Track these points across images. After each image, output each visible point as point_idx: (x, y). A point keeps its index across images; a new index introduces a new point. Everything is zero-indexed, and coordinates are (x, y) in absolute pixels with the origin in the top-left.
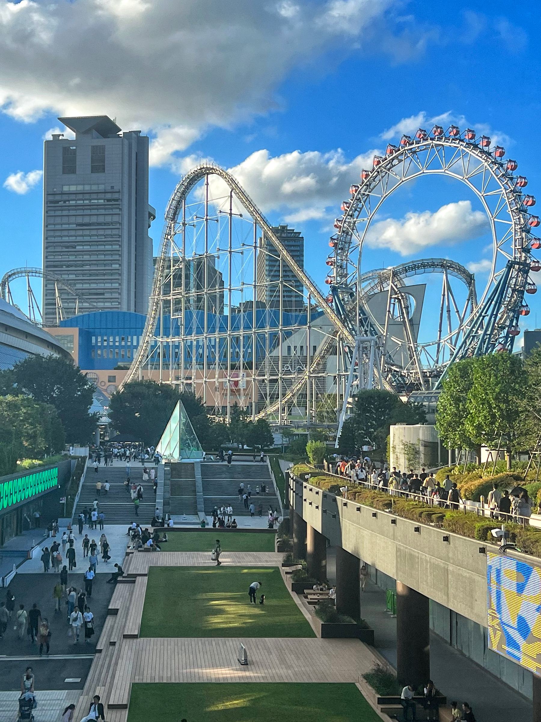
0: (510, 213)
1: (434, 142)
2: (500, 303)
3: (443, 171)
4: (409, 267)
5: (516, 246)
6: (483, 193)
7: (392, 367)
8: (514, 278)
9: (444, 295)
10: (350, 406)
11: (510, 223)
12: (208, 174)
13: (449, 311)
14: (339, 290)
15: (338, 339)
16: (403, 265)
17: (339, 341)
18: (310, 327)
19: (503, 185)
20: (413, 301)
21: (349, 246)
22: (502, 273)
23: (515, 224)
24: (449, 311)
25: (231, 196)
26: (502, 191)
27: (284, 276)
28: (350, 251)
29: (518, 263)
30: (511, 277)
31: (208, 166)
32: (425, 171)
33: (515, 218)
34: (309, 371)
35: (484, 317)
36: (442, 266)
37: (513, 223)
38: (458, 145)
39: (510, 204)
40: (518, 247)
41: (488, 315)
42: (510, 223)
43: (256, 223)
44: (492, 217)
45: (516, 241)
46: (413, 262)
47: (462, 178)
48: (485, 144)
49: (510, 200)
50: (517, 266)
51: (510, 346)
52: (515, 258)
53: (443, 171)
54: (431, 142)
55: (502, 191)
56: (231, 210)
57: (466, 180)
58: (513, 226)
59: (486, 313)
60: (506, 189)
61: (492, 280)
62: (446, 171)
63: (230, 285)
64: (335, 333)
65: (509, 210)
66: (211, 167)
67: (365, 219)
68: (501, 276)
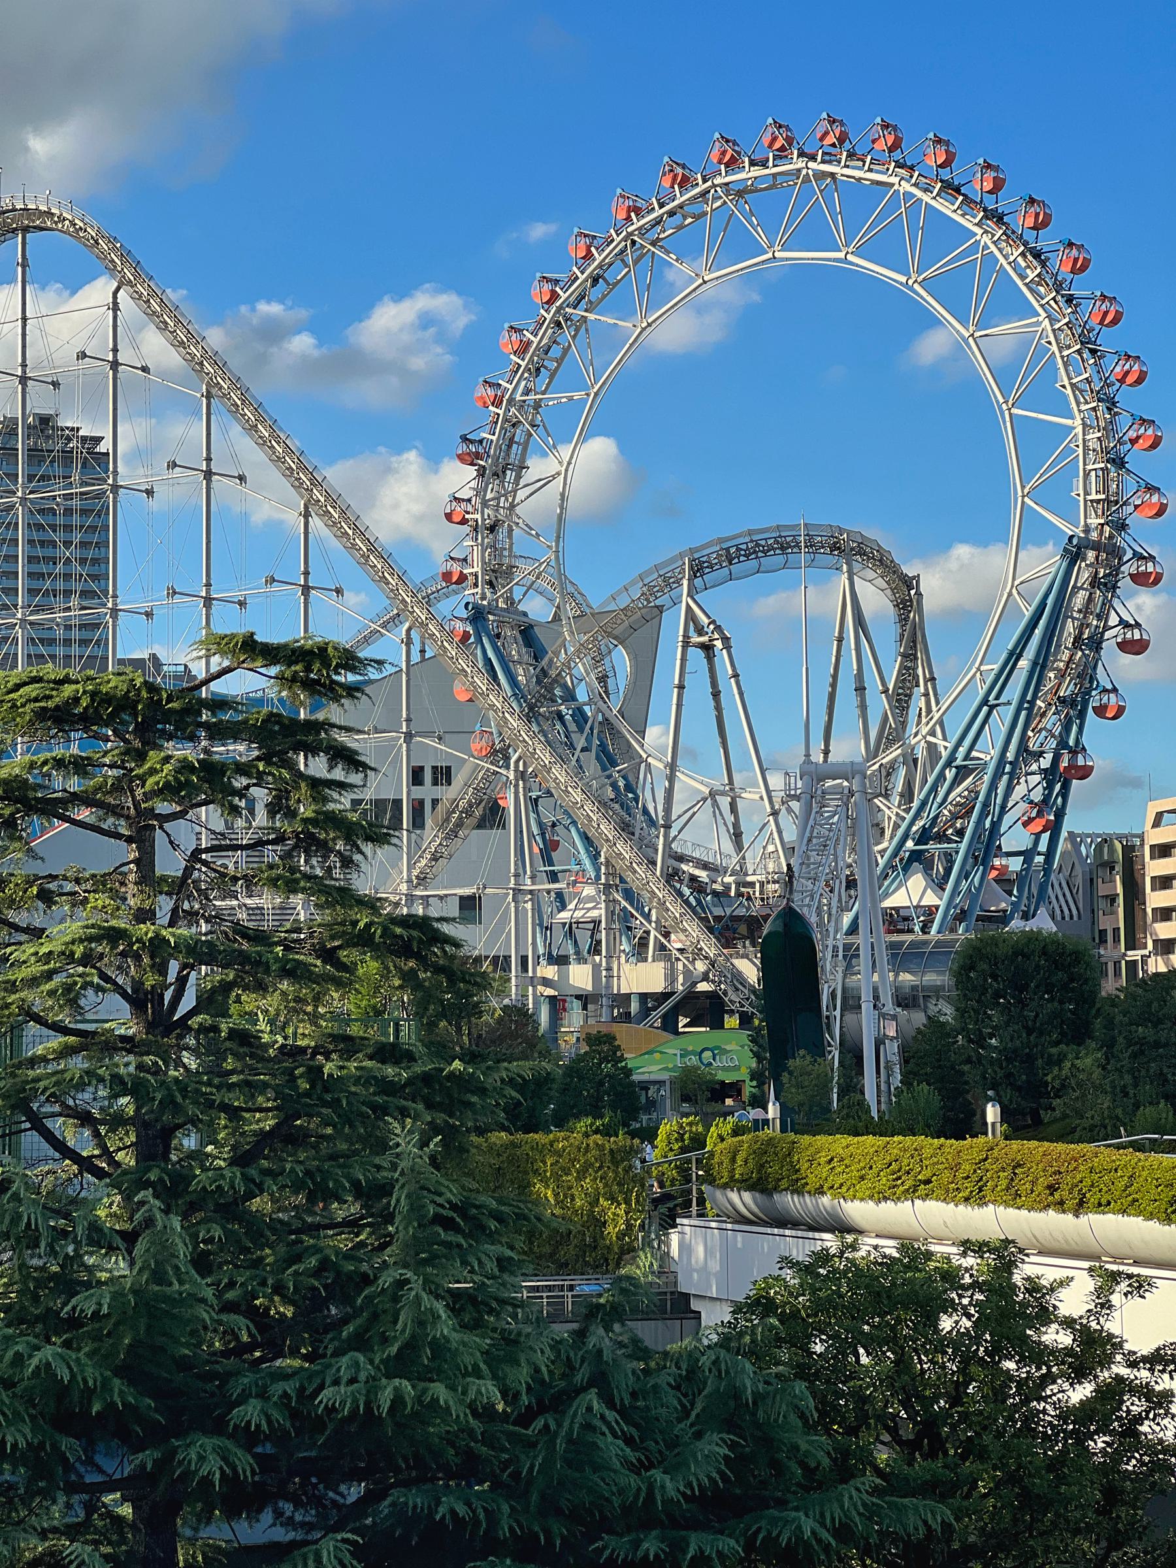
0: (1069, 391)
1: (811, 165)
2: (1043, 667)
3: (841, 255)
4: (738, 550)
5: (1087, 493)
6: (971, 329)
7: (684, 867)
8: (1081, 588)
9: (840, 640)
10: (550, 992)
11: (1069, 422)
12: (26, 230)
13: (861, 689)
14: (491, 617)
15: (512, 777)
16: (721, 540)
17: (517, 781)
18: (409, 736)
19: (1042, 306)
21: (519, 477)
22: (1053, 570)
23: (1084, 425)
24: (861, 689)
25: (115, 307)
26: (1038, 323)
27: (32, 592)
28: (521, 495)
29: (1096, 546)
30: (1074, 587)
31: (32, 206)
32: (849, 257)
33: (1083, 407)
34: (409, 881)
35: (992, 707)
36: (835, 547)
37: (1078, 422)
38: (894, 180)
39: (1066, 365)
40: (1094, 497)
41: (1009, 703)
42: (1069, 422)
43: (209, 396)
44: (1006, 402)
45: (1087, 475)
46: (750, 532)
47: (903, 279)
48: (988, 186)
49: (1065, 353)
50: (1091, 555)
51: (1060, 800)
52: (1087, 530)
53: (841, 255)
54: (800, 164)
55: (1038, 323)
56: (115, 350)
57: (916, 286)
58: (1079, 430)
59: (997, 698)
60: (1052, 320)
61: (1010, 594)
62: (849, 257)
63: (208, 585)
64: (500, 754)
65: (1066, 382)
66: (43, 208)
67: (577, 395)
68: (1050, 576)
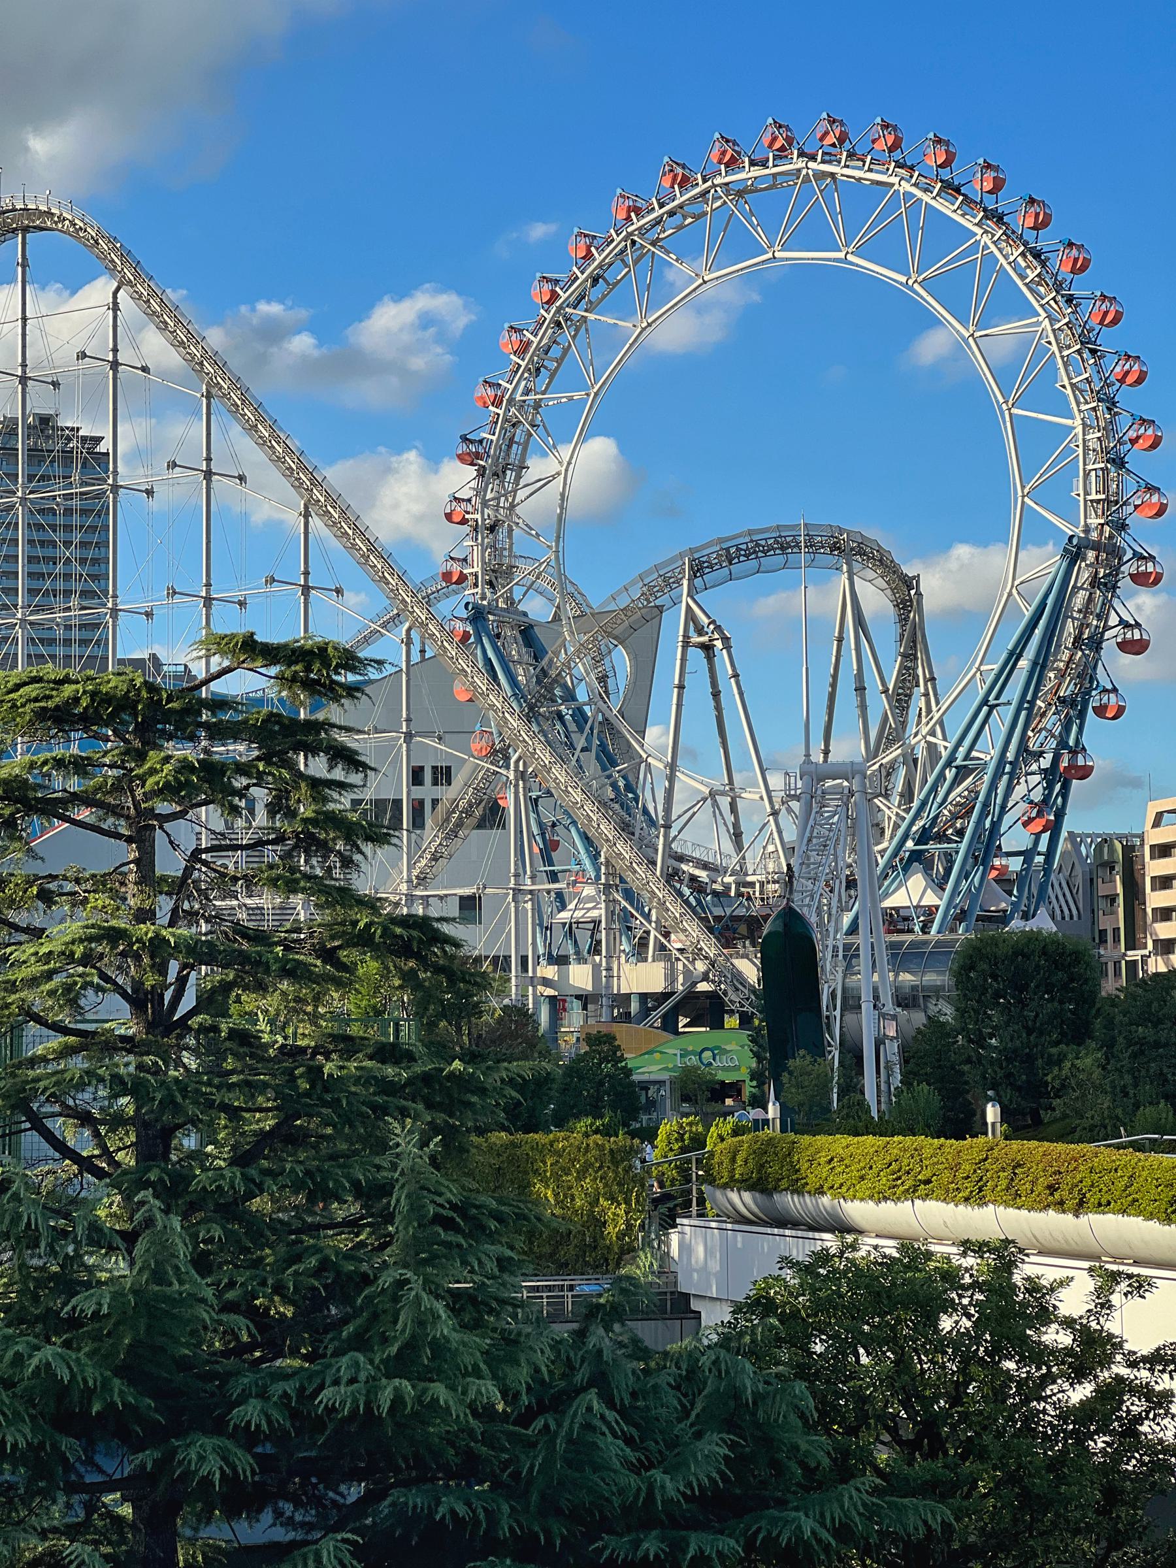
0: (1069, 391)
1: (811, 165)
2: (1043, 667)
3: (841, 255)
4: (738, 550)
5: (1087, 493)
6: (971, 329)
7: (684, 867)
8: (1081, 588)
9: (840, 640)
10: (550, 992)
11: (1069, 422)
12: (26, 230)
13: (861, 689)
14: (491, 617)
15: (512, 777)
16: (721, 540)
17: (517, 781)
18: (409, 736)
19: (1042, 306)
20: (622, 661)
21: (519, 477)
22: (1053, 570)
23: (1084, 425)
24: (861, 689)
25: (115, 307)
26: (1038, 323)
27: (32, 592)
28: (521, 495)
29: (1096, 546)
30: (1074, 587)
31: (32, 206)
33: (1083, 407)
34: (409, 881)
35: (992, 707)
36: (835, 547)
37: (1078, 422)
38: (894, 180)
39: (1066, 365)
40: (1094, 497)
41: (1009, 703)
42: (1069, 422)
43: (209, 396)
44: (1006, 402)
45: (1087, 475)
46: (750, 532)
47: (903, 279)
49: (1065, 353)
50: (1091, 555)
51: (1060, 800)
52: (1087, 530)
53: (841, 255)
54: (800, 164)
55: (1038, 323)
56: (115, 350)
57: (916, 286)
58: (1079, 430)
59: (997, 698)
60: (1052, 320)
61: (1010, 594)
62: (849, 257)
63: (208, 585)
64: (500, 754)
65: (1066, 382)
66: (43, 208)
67: (577, 395)
